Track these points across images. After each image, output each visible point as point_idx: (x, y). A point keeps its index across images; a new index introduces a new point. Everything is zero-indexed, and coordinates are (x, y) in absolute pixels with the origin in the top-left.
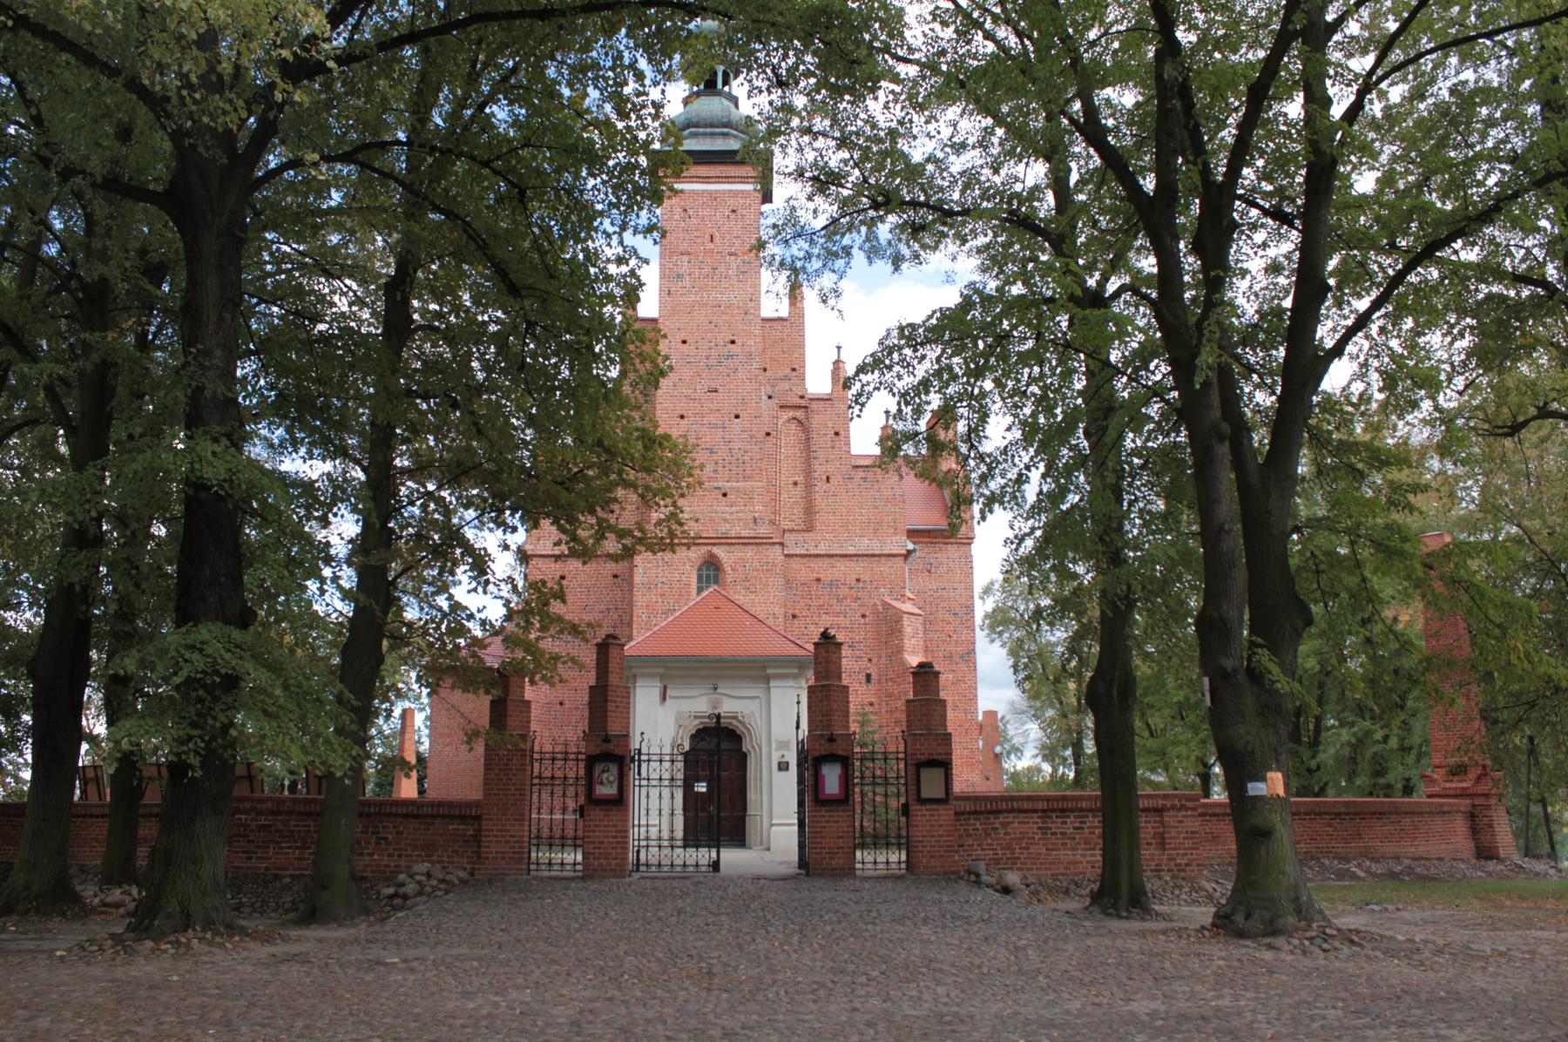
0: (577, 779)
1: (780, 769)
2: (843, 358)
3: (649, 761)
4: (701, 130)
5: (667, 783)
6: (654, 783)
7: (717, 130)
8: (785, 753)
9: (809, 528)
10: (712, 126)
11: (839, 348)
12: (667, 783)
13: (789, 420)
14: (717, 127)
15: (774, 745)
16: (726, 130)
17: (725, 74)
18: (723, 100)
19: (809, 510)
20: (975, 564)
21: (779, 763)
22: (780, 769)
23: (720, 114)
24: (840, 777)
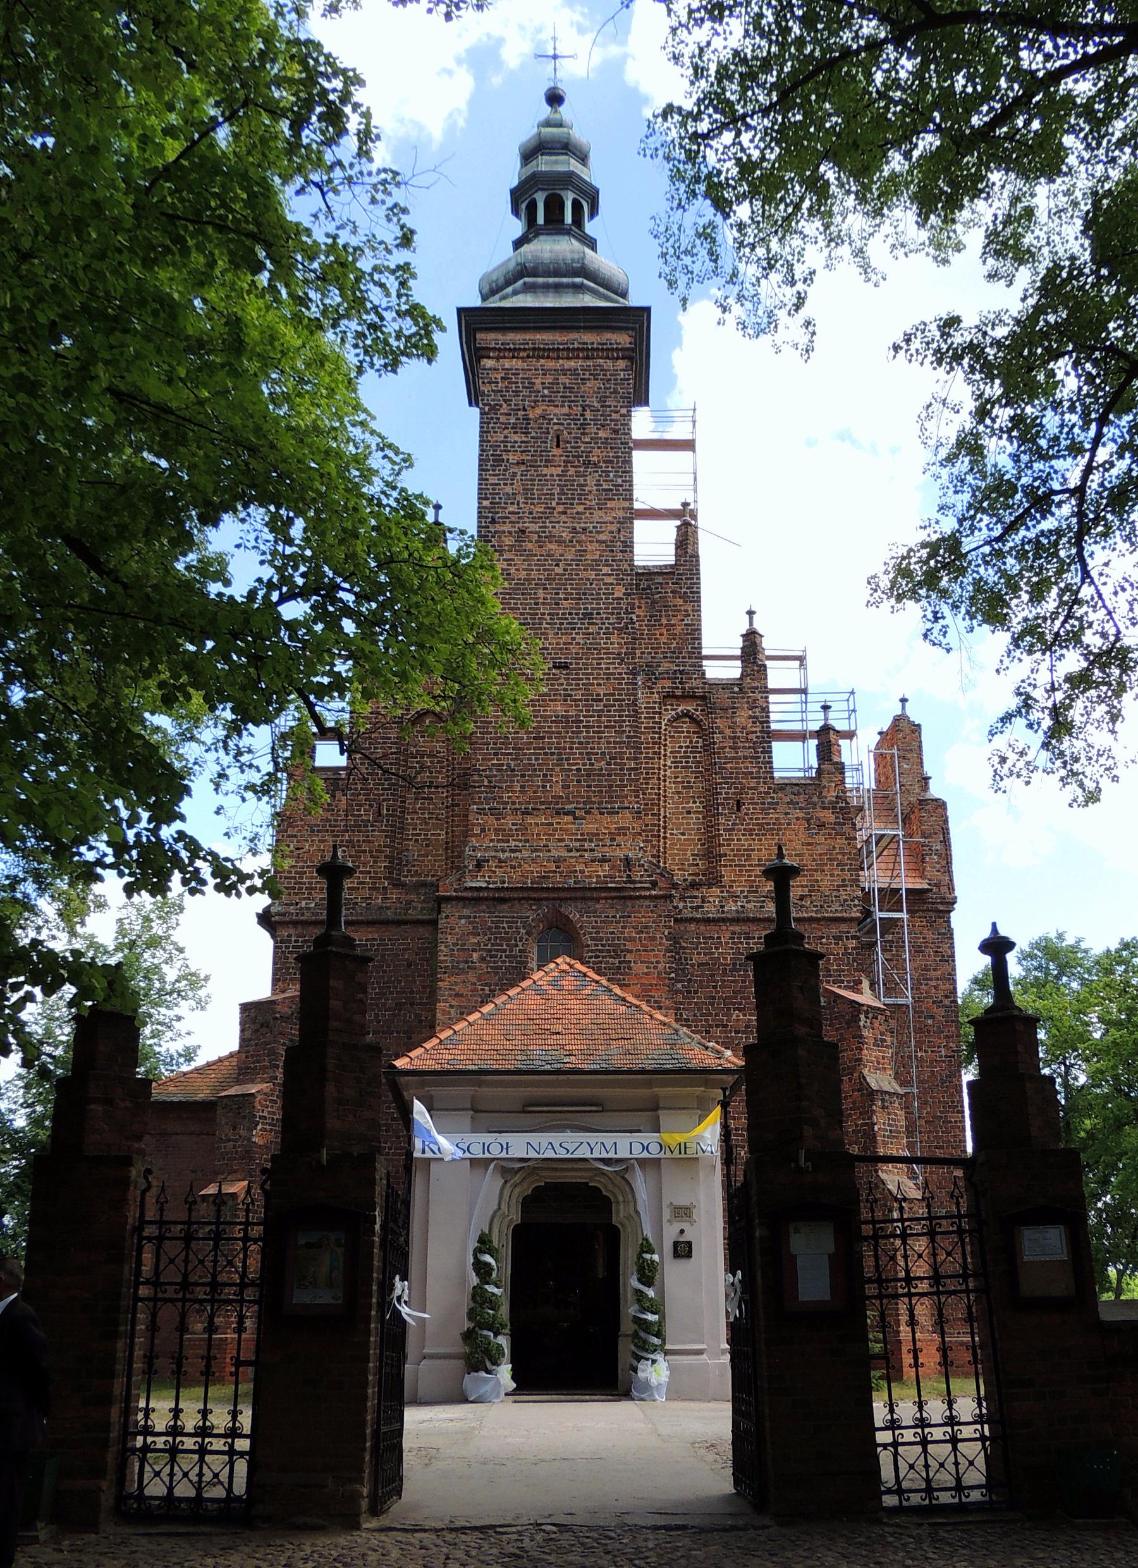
0: (243, 1285)
1: (677, 1254)
2: (758, 626)
3: (895, 1444)
4: (540, 280)
5: (924, 1286)
6: (170, 1292)
7: (565, 280)
8: (685, 1226)
9: (714, 880)
10: (557, 273)
11: (751, 613)
12: (924, 1286)
13: (678, 718)
14: (565, 276)
15: (667, 1214)
16: (578, 280)
17: (577, 207)
18: (573, 241)
19: (711, 854)
20: (955, 936)
21: (676, 1244)
22: (677, 1254)
23: (569, 256)
24: (831, 1257)
